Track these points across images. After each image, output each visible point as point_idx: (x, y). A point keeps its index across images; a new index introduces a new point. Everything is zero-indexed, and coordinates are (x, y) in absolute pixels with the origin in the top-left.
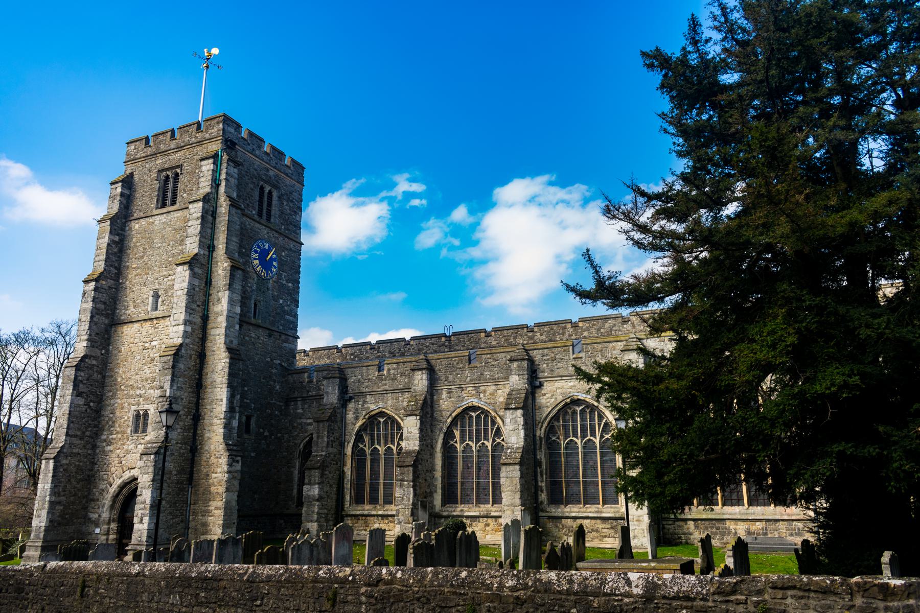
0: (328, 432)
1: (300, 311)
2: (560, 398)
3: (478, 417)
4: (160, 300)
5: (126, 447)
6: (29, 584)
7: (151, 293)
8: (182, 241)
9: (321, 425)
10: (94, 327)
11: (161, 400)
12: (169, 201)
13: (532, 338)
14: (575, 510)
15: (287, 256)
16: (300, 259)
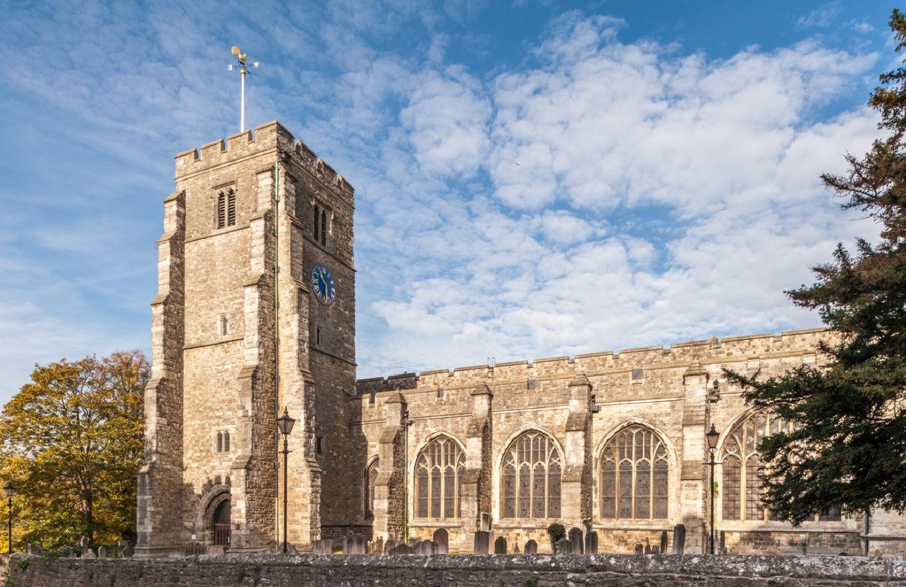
0: (394, 453)
1: (356, 339)
2: (617, 422)
3: (535, 439)
4: (228, 324)
5: (211, 464)
6: (184, 575)
7: (219, 317)
8: (246, 263)
9: (386, 446)
10: (168, 351)
11: (244, 419)
12: (226, 221)
13: (573, 369)
14: (626, 523)
15: (343, 283)
16: (354, 287)
